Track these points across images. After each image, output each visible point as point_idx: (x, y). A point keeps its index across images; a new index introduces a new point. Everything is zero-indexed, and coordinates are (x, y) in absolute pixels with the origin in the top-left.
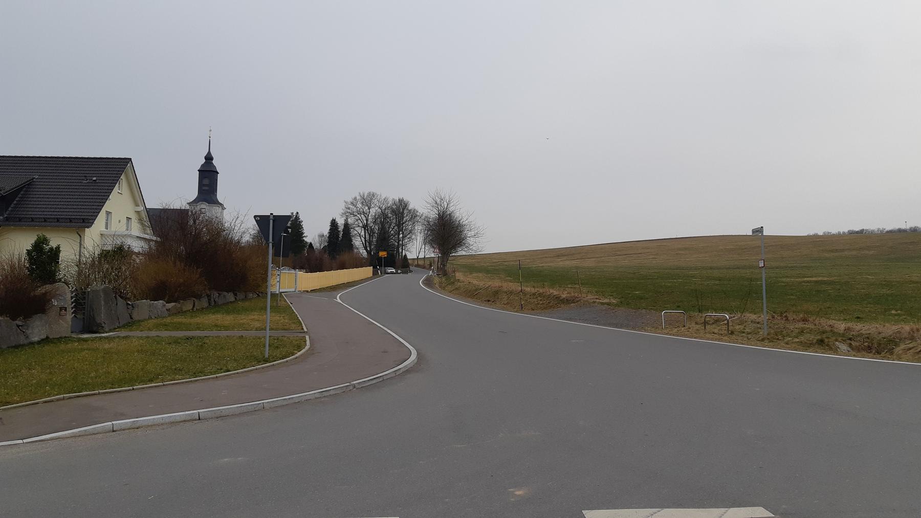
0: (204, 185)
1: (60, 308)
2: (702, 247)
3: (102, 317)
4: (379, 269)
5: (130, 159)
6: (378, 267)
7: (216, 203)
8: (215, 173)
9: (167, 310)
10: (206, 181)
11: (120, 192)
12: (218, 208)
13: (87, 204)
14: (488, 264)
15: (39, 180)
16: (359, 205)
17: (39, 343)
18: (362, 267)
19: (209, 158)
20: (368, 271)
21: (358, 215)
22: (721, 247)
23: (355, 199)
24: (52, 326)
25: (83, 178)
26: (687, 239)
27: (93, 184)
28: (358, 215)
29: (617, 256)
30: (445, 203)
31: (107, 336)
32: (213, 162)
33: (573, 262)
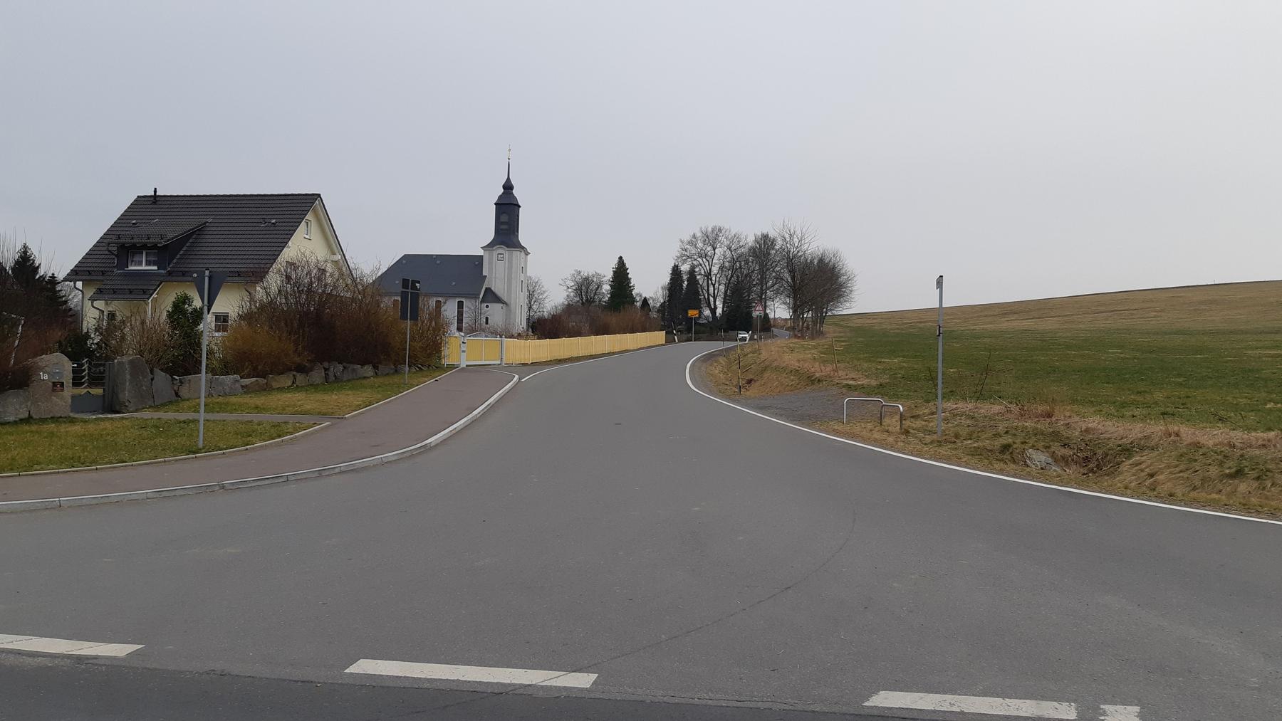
0: (503, 223)
1: (54, 383)
2: (1241, 298)
3: (126, 394)
4: (675, 334)
5: (319, 195)
6: (675, 332)
7: (518, 246)
8: (516, 207)
9: (242, 386)
10: (504, 218)
11: (307, 237)
12: (519, 252)
13: (264, 248)
14: (894, 326)
15: (212, 225)
16: (700, 245)
17: (15, 423)
18: (644, 331)
19: (508, 187)
20: (660, 336)
21: (699, 259)
22: (1272, 299)
23: (694, 236)
24: (40, 403)
25: (262, 221)
26: (1169, 290)
27: (271, 228)
28: (699, 259)
29: (1097, 313)
30: (795, 239)
31: (115, 413)
32: (514, 191)
33: (1025, 323)
